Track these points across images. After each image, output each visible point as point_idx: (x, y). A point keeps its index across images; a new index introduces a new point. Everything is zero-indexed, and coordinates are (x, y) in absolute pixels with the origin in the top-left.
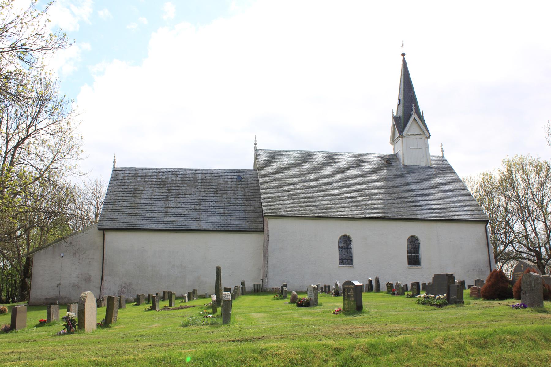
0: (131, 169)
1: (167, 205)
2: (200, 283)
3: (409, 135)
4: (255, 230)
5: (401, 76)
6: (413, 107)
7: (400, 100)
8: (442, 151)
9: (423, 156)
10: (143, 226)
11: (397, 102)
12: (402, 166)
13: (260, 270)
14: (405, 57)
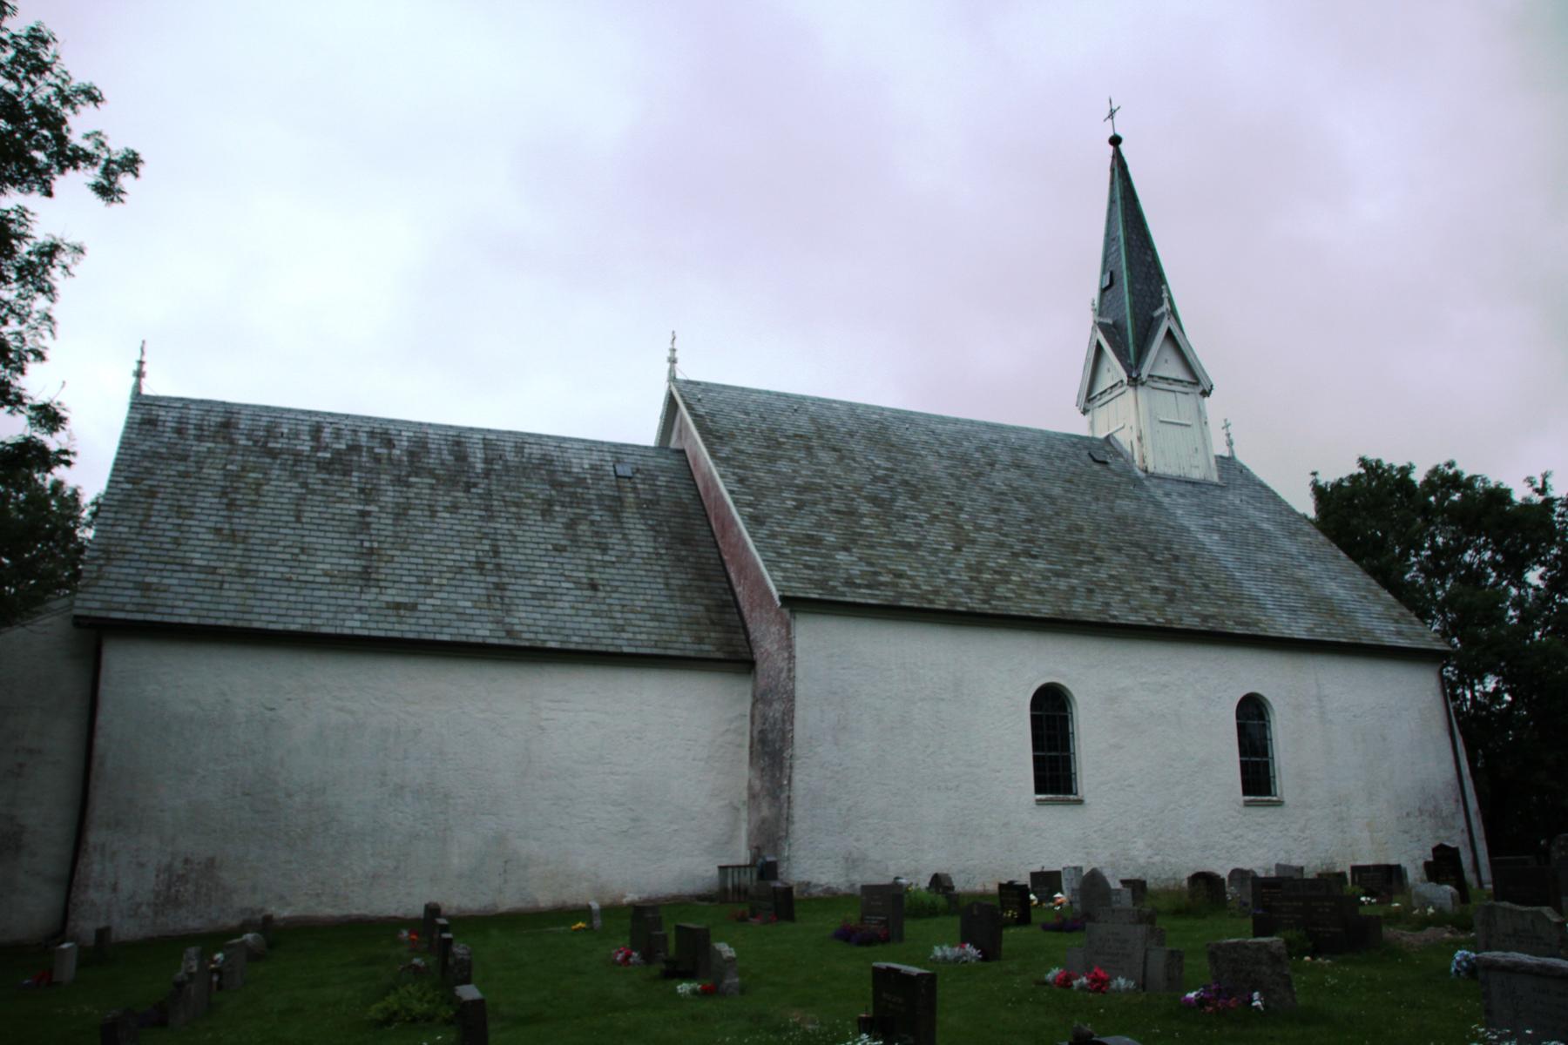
0: (207, 406)
1: (367, 544)
2: (506, 862)
3: (1156, 379)
8: (1230, 444)
9: (1196, 449)
10: (274, 618)
12: (1141, 474)
13: (737, 809)
14: (1122, 146)
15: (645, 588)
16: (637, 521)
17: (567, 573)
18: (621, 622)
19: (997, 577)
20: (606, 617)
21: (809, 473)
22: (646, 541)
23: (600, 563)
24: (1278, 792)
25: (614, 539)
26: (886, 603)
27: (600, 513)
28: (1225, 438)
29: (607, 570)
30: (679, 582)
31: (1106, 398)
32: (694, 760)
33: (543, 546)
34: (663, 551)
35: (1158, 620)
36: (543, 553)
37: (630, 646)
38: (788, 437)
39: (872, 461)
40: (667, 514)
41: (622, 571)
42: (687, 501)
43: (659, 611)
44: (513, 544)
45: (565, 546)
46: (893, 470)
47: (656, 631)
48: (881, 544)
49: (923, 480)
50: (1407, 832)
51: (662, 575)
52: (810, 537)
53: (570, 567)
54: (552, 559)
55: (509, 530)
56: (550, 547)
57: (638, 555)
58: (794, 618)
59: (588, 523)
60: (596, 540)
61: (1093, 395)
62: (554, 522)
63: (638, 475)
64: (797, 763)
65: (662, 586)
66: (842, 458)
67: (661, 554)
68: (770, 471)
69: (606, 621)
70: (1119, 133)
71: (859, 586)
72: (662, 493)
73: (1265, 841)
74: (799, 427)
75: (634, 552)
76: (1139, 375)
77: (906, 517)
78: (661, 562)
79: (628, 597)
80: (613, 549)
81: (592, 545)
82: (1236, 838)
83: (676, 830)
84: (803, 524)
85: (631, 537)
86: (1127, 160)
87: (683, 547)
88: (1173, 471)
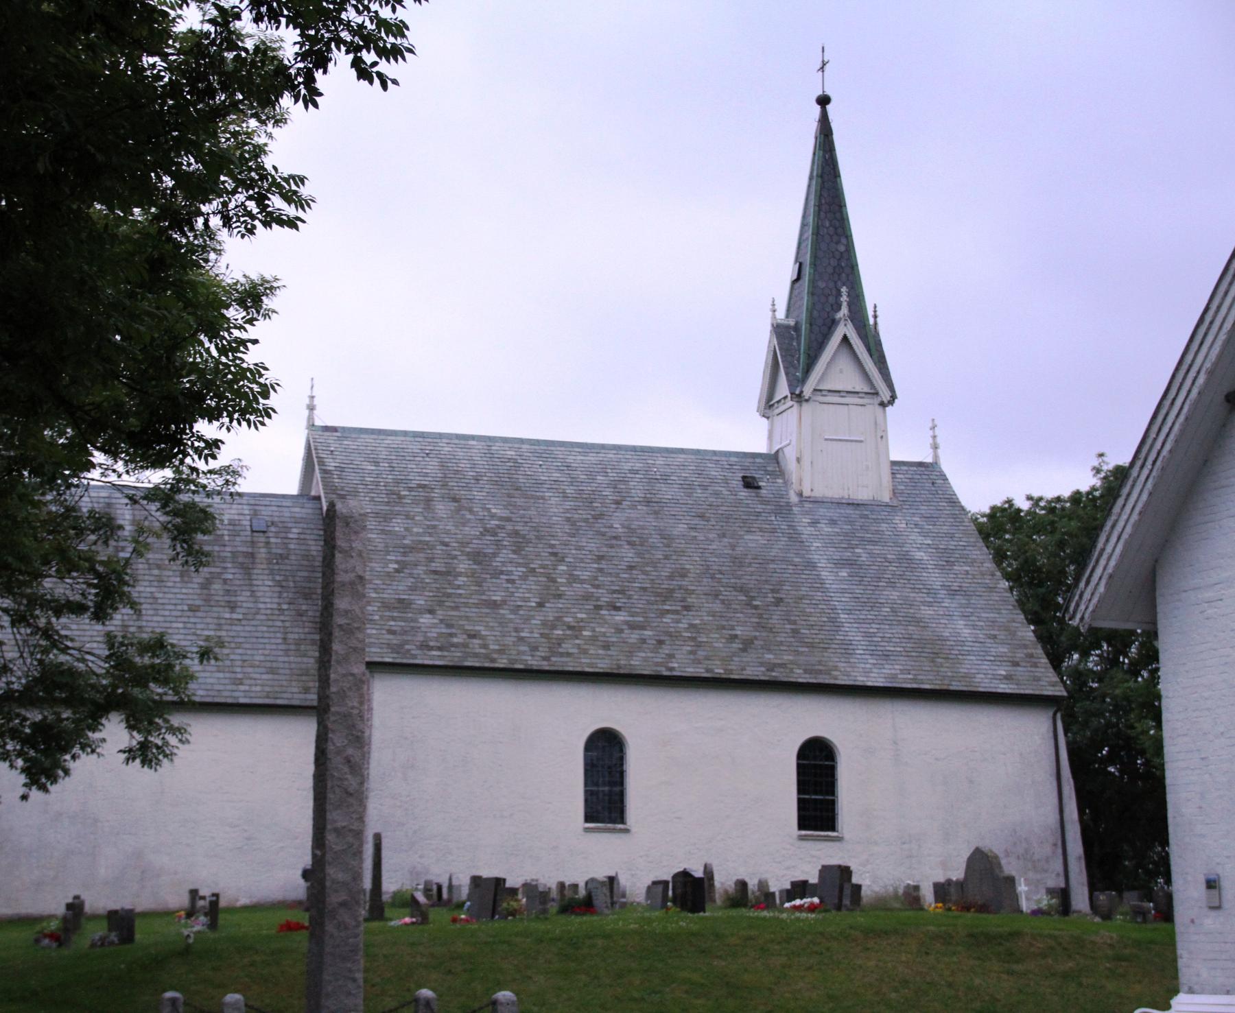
5: (811, 178)
6: (844, 299)
7: (801, 265)
8: (935, 447)
11: (788, 271)
12: (794, 498)
14: (829, 107)
15: (264, 644)
16: (266, 577)
17: (199, 632)
18: (239, 676)
19: (568, 632)
20: (229, 672)
21: (421, 530)
22: (271, 597)
23: (229, 622)
24: (840, 828)
25: (243, 597)
26: (450, 664)
27: (233, 571)
28: (931, 440)
29: (234, 628)
30: (296, 636)
31: (782, 408)
32: (298, 790)
33: (179, 607)
34: (285, 607)
35: (716, 671)
36: (179, 614)
37: (245, 697)
38: (410, 489)
39: (489, 510)
40: (295, 567)
41: (248, 628)
42: (315, 553)
43: (274, 665)
44: (155, 606)
45: (199, 606)
46: (509, 519)
47: (269, 683)
48: (466, 605)
49: (536, 529)
51: (282, 630)
52: (401, 601)
53: (202, 626)
54: (186, 620)
55: (151, 593)
56: (186, 608)
57: (263, 611)
58: (373, 677)
59: (221, 581)
60: (227, 598)
61: (772, 403)
62: (192, 582)
63: (273, 529)
64: (371, 795)
65: (280, 641)
66: (458, 510)
67: (284, 610)
68: (383, 532)
69: (228, 675)
70: (828, 92)
71: (432, 648)
72: (292, 546)
74: (426, 475)
75: (260, 609)
76: (802, 392)
77: (502, 573)
78: (282, 618)
79: (249, 652)
80: (241, 607)
81: (223, 604)
82: (788, 868)
83: (283, 847)
84: (401, 587)
85: (259, 594)
86: (834, 126)
87: (305, 602)
88: (834, 491)
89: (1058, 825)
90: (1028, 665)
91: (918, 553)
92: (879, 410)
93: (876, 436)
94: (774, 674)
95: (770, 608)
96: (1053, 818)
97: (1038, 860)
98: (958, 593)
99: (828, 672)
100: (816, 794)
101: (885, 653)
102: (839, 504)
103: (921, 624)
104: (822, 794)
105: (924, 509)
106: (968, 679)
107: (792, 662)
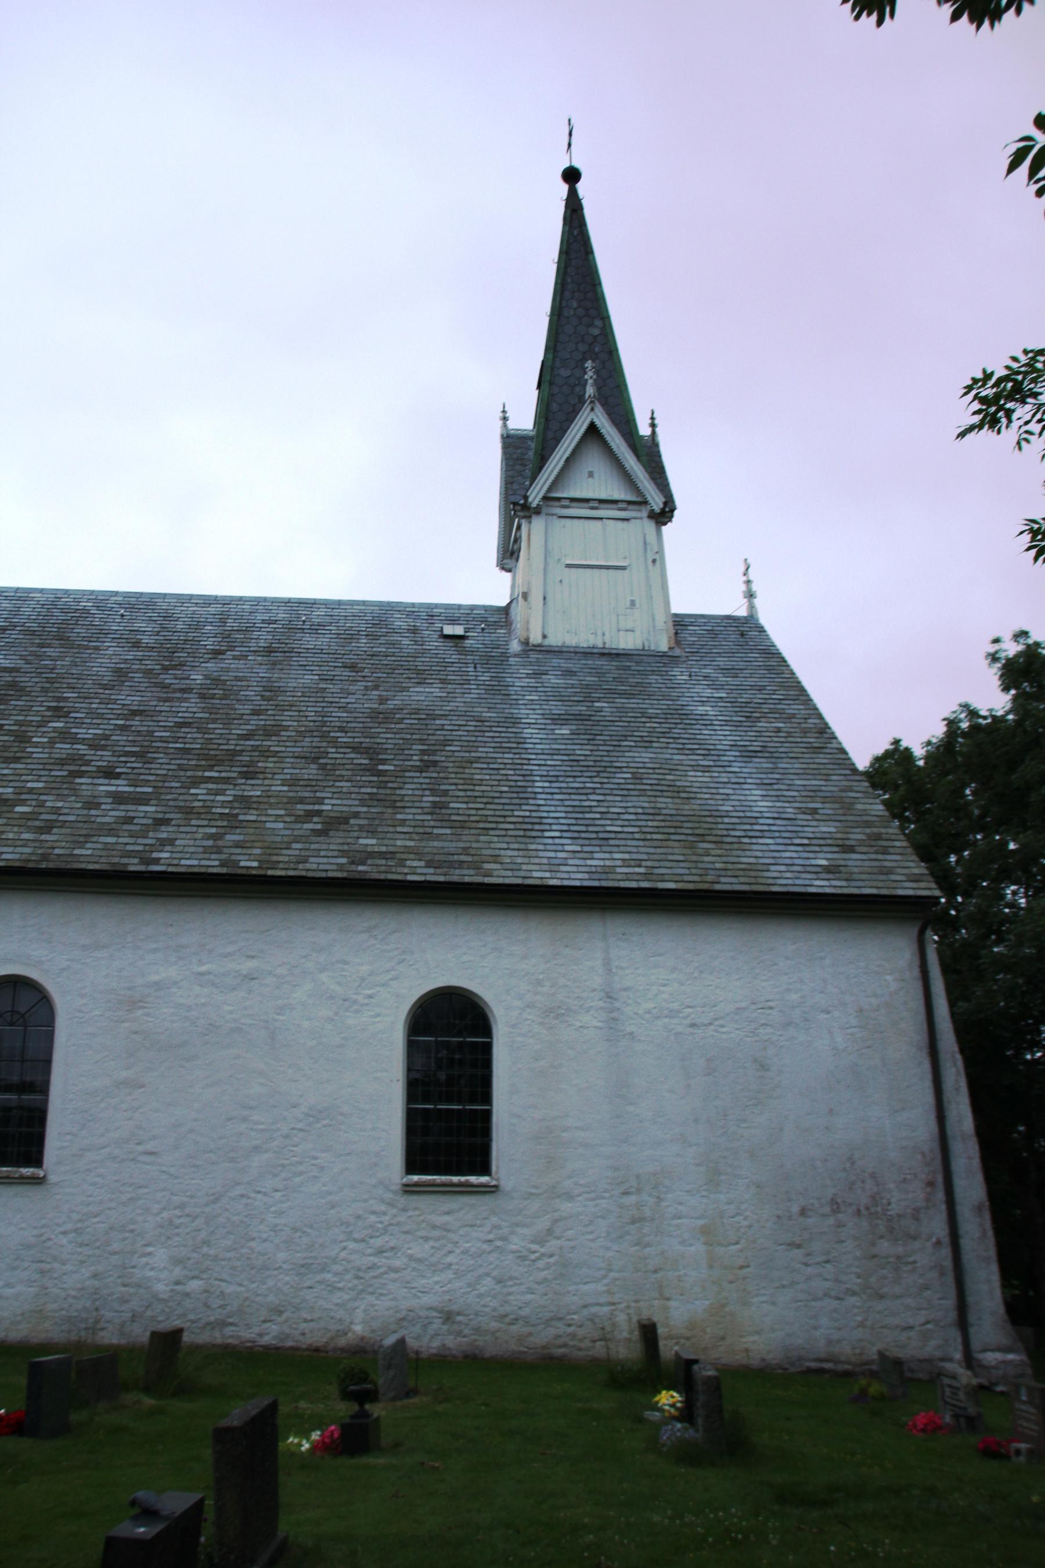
3: (567, 503)
4: (33, 1010)
8: (750, 595)
9: (633, 603)
24: (494, 1168)
50: (799, 1246)
70: (576, 164)
73: (450, 1259)
82: (380, 1252)
88: (585, 639)
89: (936, 1146)
90: (872, 850)
91: (700, 708)
92: (650, 526)
93: (646, 560)
94: (361, 868)
95: (407, 774)
96: (925, 1129)
97: (899, 1216)
98: (760, 754)
99: (476, 866)
100: (450, 1100)
101: (601, 835)
102: (588, 653)
103: (682, 795)
104: (459, 1102)
105: (722, 662)
106: (752, 873)
107: (408, 850)
